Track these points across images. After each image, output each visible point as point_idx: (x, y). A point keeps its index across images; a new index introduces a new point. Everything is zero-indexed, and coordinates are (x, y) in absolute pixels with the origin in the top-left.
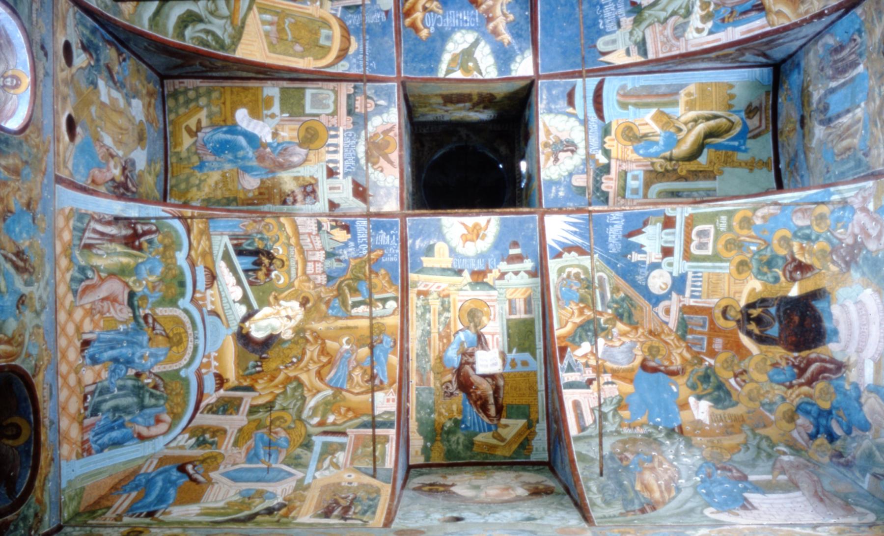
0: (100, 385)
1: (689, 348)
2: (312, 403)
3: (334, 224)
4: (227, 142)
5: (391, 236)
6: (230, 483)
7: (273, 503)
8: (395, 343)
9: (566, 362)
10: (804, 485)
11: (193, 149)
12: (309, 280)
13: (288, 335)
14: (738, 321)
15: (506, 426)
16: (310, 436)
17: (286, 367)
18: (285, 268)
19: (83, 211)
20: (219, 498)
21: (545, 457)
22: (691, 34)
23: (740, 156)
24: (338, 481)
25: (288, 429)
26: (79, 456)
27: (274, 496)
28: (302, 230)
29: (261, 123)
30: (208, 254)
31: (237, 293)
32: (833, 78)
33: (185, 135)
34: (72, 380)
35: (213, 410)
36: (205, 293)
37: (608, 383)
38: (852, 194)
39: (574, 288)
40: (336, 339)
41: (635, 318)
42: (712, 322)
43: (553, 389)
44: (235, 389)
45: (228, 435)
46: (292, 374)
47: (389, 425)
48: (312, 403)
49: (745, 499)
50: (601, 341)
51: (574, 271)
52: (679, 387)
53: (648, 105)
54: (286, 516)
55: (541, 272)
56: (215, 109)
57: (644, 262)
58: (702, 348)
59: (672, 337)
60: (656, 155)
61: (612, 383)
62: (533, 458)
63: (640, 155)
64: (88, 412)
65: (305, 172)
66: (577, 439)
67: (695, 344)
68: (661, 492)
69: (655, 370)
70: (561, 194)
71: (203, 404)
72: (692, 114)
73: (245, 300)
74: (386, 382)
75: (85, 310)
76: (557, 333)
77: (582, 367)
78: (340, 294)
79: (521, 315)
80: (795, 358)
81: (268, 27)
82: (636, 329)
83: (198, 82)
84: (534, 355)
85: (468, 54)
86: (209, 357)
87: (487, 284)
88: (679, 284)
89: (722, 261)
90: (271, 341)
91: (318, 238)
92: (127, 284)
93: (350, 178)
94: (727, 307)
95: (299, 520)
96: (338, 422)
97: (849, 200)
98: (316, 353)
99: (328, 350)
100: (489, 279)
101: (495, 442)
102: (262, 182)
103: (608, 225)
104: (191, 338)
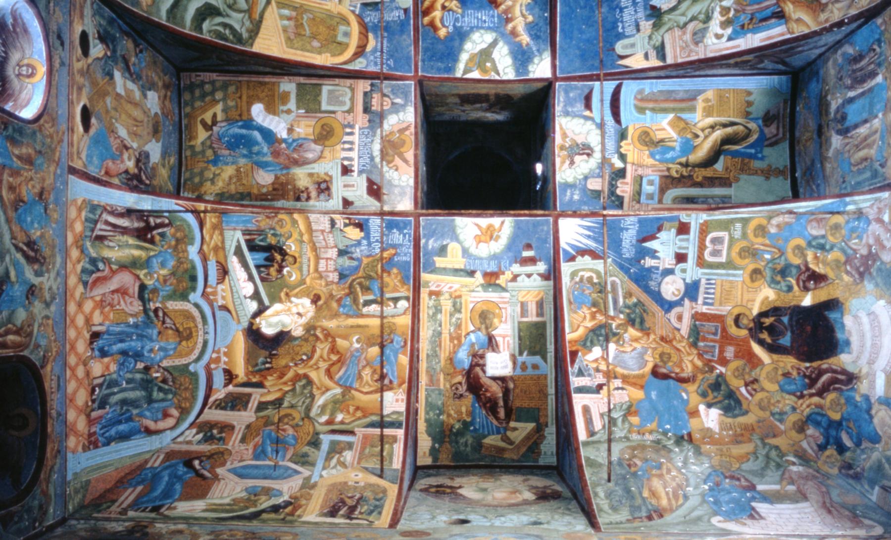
0: (108, 377)
1: (700, 356)
2: (320, 401)
3: (347, 221)
4: (243, 136)
5: (404, 235)
6: (237, 479)
7: (280, 501)
8: (405, 343)
9: (576, 366)
11: (208, 143)
13: (298, 332)
14: (750, 330)
15: (515, 429)
16: (318, 434)
17: (296, 365)
18: (297, 264)
19: (96, 203)
20: (225, 495)
22: (710, 40)
23: (757, 164)
25: (295, 427)
26: (86, 449)
27: (280, 493)
28: (314, 227)
29: (277, 118)
30: (220, 249)
31: (248, 289)
32: (851, 88)
33: (200, 128)
34: (80, 372)
35: (221, 405)
36: (216, 288)
37: (618, 389)
38: (868, 204)
39: (587, 292)
40: (346, 337)
41: (647, 325)
42: (724, 330)
44: (244, 385)
46: (301, 372)
49: (753, 509)
50: (612, 347)
51: (587, 274)
52: (690, 394)
54: (292, 514)
55: (553, 275)
57: (657, 268)
58: (713, 356)
59: (683, 344)
60: (672, 161)
61: (622, 389)
62: (541, 462)
64: (96, 405)
65: (320, 168)
66: (586, 444)
67: (707, 352)
68: (669, 499)
69: (666, 377)
70: (576, 197)
71: (212, 399)
72: (710, 121)
73: (256, 296)
74: (395, 382)
75: (96, 302)
76: (569, 336)
77: (592, 372)
78: (351, 292)
79: (532, 318)
80: (807, 368)
81: (286, 22)
82: (648, 335)
83: (214, 76)
84: (544, 358)
85: (486, 54)
86: (218, 352)
87: (499, 285)
88: (691, 290)
89: (735, 268)
90: (282, 337)
91: (331, 235)
93: (364, 176)
96: (347, 421)
97: (864, 211)
100: (502, 281)
101: (503, 444)
102: (277, 178)
103: (622, 229)
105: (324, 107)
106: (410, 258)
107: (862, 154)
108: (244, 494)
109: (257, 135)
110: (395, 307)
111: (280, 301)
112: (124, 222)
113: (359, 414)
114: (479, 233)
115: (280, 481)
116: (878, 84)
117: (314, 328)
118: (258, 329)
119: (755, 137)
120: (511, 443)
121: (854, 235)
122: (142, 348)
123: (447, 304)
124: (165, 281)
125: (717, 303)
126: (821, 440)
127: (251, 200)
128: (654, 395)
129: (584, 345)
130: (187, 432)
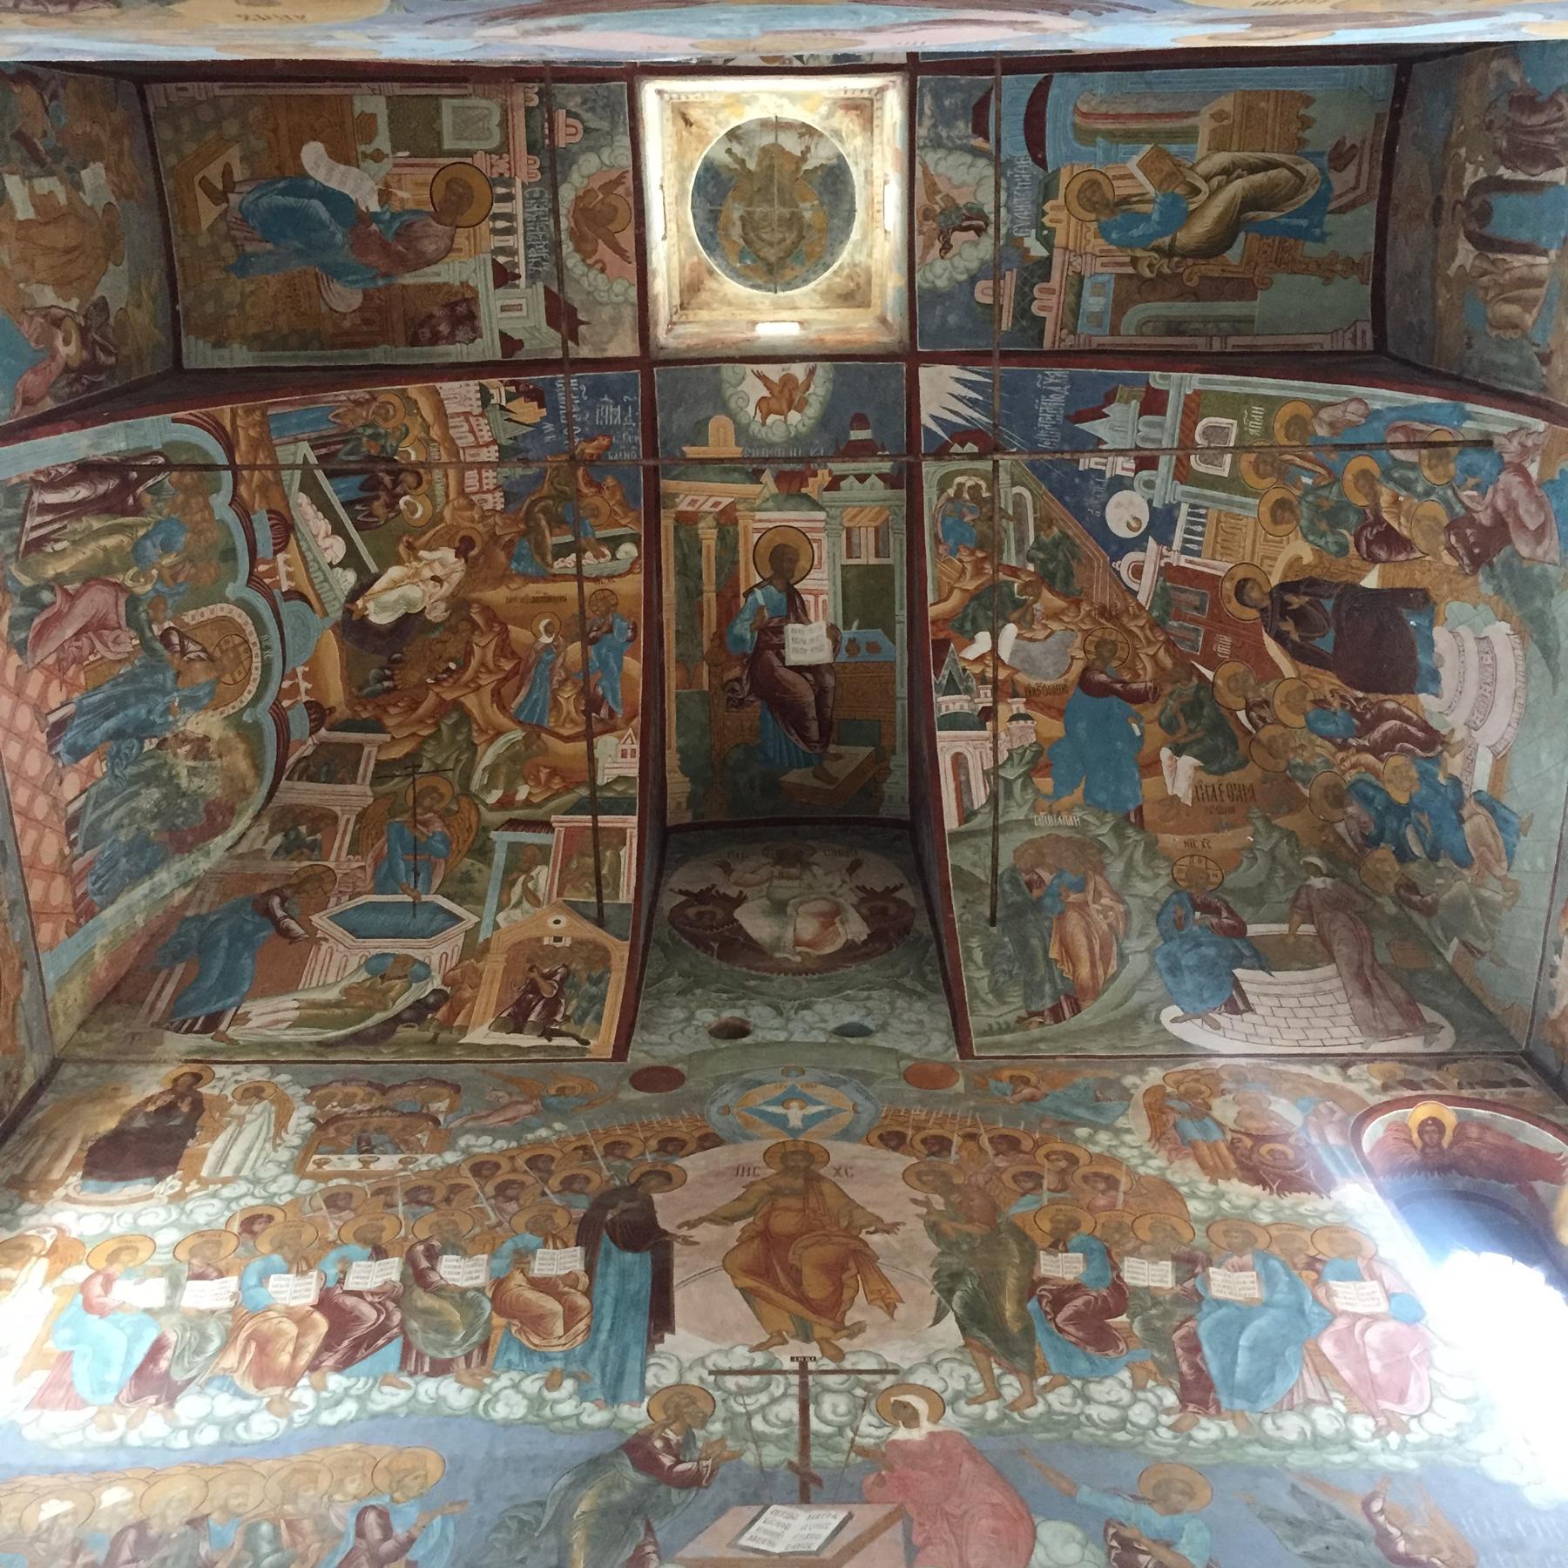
0: (93, 791)
1: (1170, 645)
2: (487, 758)
3: (512, 389)
4: (291, 210)
5: (624, 409)
6: (349, 939)
8: (635, 630)
9: (945, 672)
10: (1341, 950)
11: (222, 227)
12: (472, 505)
13: (437, 614)
14: (1263, 611)
17: (438, 682)
18: (424, 486)
19: (15, 481)
20: (331, 979)
21: (905, 813)
23: (1311, 249)
24: (536, 933)
25: (445, 815)
27: (425, 971)
28: (451, 408)
29: (354, 170)
30: (272, 487)
32: (1507, 159)
33: (203, 201)
35: (310, 770)
36: (274, 560)
37: (1016, 717)
38: (1506, 429)
39: (968, 518)
40: (526, 622)
42: (1216, 602)
43: (922, 726)
45: (342, 823)
46: (449, 696)
47: (619, 806)
48: (487, 758)
49: (1236, 984)
50: (1010, 631)
51: (969, 482)
52: (1145, 725)
53: (1132, 137)
54: (447, 1025)
55: (907, 480)
56: (260, 145)
57: (1101, 473)
58: (1194, 648)
59: (1141, 622)
60: (1143, 243)
61: (1026, 717)
62: (884, 813)
63: (1111, 242)
65: (448, 273)
66: (957, 837)
68: (1093, 965)
69: (1104, 690)
70: (952, 319)
71: (291, 761)
72: (1222, 158)
73: (352, 559)
74: (620, 713)
75: (48, 668)
76: (933, 612)
77: (973, 684)
78: (531, 531)
79: (868, 558)
80: (1358, 700)
82: (1077, 604)
84: (890, 634)
86: (294, 675)
87: (806, 496)
88: (1161, 523)
89: (1245, 494)
90: (410, 624)
91: (483, 421)
92: (120, 587)
93: (540, 287)
94: (1246, 580)
95: (469, 1038)
96: (536, 800)
97: (1496, 440)
98: (490, 655)
99: (515, 647)
100: (812, 488)
101: (817, 783)
102: (367, 296)
104: (256, 650)
105: (448, 145)
107: (1512, 310)
108: (364, 975)
109: (317, 206)
110: (614, 558)
111: (399, 562)
112: (81, 492)
113: (557, 784)
114: (766, 393)
115: (423, 942)
116: (1555, 184)
118: (364, 618)
119: (1311, 193)
121: (1471, 482)
122: (150, 712)
123: (708, 534)
124: (174, 577)
125: (1207, 551)
126: (1372, 830)
127: (322, 348)
128: (1081, 727)
129: (961, 630)
130: (253, 833)
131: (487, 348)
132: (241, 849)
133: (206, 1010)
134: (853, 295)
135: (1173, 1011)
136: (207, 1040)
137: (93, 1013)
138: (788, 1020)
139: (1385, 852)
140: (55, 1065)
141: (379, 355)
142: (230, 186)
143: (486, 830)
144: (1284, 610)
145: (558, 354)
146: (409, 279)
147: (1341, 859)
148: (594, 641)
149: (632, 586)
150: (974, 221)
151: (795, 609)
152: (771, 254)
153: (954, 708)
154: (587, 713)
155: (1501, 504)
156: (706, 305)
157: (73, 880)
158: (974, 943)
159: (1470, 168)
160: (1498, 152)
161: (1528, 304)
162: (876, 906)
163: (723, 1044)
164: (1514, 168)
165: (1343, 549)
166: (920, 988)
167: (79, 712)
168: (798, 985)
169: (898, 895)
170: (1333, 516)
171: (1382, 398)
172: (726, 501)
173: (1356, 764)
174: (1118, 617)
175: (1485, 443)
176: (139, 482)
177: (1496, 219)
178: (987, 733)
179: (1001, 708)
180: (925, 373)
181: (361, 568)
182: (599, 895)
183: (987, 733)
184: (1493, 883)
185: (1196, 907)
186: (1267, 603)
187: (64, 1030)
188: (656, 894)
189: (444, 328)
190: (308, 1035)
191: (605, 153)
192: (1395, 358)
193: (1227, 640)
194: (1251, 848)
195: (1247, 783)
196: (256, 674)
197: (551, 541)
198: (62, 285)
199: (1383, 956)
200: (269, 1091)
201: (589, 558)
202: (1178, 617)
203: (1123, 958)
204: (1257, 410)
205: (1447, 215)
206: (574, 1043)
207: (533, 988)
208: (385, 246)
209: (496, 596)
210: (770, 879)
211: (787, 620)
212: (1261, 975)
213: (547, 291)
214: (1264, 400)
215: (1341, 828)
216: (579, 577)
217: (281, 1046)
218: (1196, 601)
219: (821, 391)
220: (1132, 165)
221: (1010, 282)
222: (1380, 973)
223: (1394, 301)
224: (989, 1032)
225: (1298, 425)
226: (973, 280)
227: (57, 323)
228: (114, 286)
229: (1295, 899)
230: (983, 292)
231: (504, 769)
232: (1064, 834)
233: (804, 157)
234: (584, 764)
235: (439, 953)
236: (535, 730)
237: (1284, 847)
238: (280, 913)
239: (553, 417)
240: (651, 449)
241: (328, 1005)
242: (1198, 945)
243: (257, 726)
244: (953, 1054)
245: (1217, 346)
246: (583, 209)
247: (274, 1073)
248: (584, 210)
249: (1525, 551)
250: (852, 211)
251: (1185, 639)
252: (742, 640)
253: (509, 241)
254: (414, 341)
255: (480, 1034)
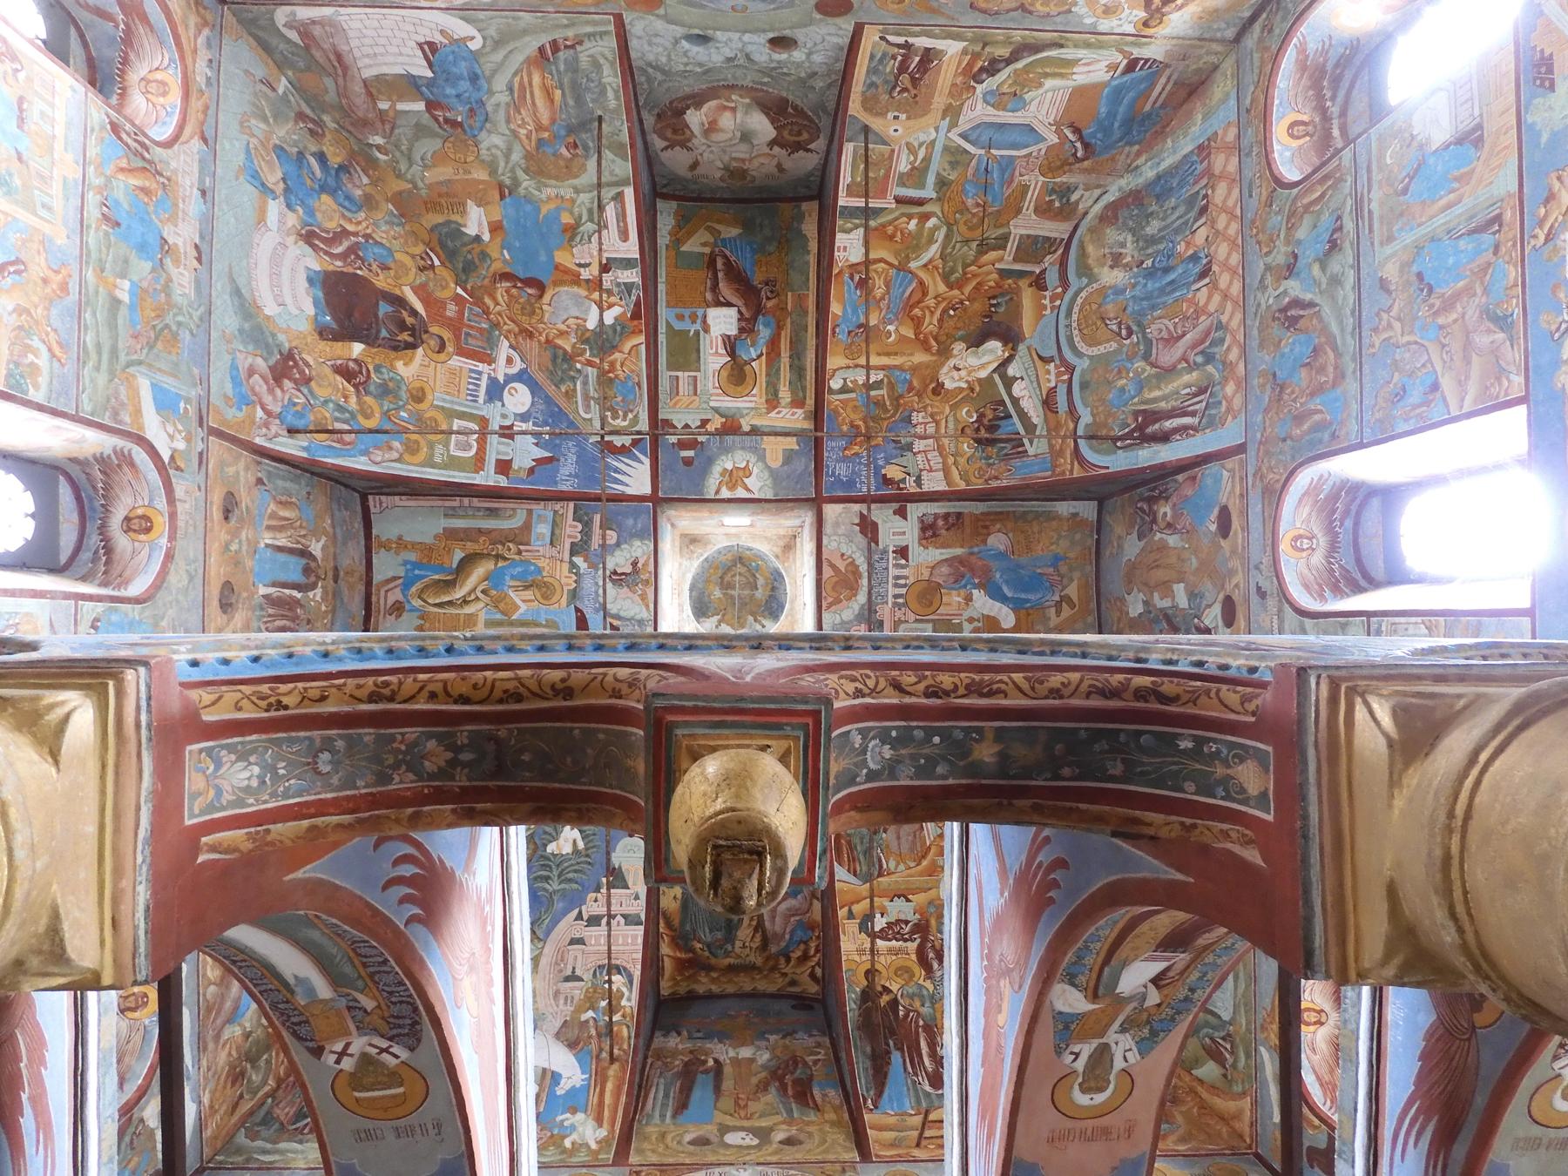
1: (487, 312)
2: (934, 250)
4: (1025, 591)
7: (991, 83)
9: (634, 298)
10: (358, 88)
11: (1065, 581)
12: (932, 416)
13: (958, 347)
14: (426, 332)
15: (704, 244)
20: (1050, 95)
21: (661, 204)
23: (413, 556)
24: (911, 123)
25: (963, 209)
30: (1053, 429)
31: (1018, 389)
32: (297, 602)
33: (1075, 599)
35: (1049, 244)
38: (280, 439)
40: (902, 339)
41: (548, 354)
42: (457, 337)
43: (648, 261)
46: (956, 292)
47: (851, 212)
48: (934, 250)
49: (431, 65)
50: (591, 324)
52: (501, 258)
54: (976, 56)
60: (514, 563)
61: (580, 265)
62: (674, 204)
65: (935, 554)
66: (625, 183)
67: (477, 315)
70: (630, 522)
72: (468, 610)
73: (1009, 382)
76: (642, 338)
77: (615, 290)
78: (896, 399)
82: (548, 341)
86: (1053, 308)
88: (496, 391)
89: (443, 408)
90: (976, 341)
92: (1153, 365)
95: (959, 46)
98: (927, 320)
101: (718, 227)
102: (984, 542)
103: (576, 476)
104: (1074, 325)
106: (829, 445)
109: (1009, 594)
111: (979, 380)
112: (1169, 424)
113: (890, 230)
117: (939, 353)
118: (1005, 344)
119: (414, 589)
120: (709, 229)
121: (299, 408)
123: (785, 394)
124: (1120, 372)
125: (465, 373)
126: (344, 177)
128: (543, 258)
131: (915, 510)
132: (1097, 192)
133: (1133, 75)
134: (691, 541)
135: (475, 45)
136: (1136, 52)
137: (1208, 77)
138: (741, 51)
139: (335, 160)
140: (1238, 39)
141: (979, 508)
142: (1058, 605)
143: (939, 199)
144: (413, 331)
145: (873, 506)
146: (958, 551)
147: (362, 158)
148: (860, 326)
149: (833, 362)
150: (618, 578)
151: (731, 345)
152: (740, 568)
153: (627, 273)
154: (868, 278)
155: (278, 392)
156: (780, 537)
157: (1209, 172)
158: (613, 104)
159: (318, 598)
160: (302, 606)
161: (273, 516)
162: (678, 135)
163: (787, 33)
164: (291, 597)
165: (378, 369)
166: (650, 70)
167: (1189, 285)
168: (734, 77)
169: (665, 144)
170: (385, 391)
171: (360, 463)
172: (773, 414)
173: (359, 223)
174: (521, 331)
175: (292, 431)
176: (1133, 431)
177: (299, 569)
178: (605, 255)
179: (596, 273)
180: (646, 490)
181: (1004, 377)
182: (867, 149)
183: (605, 255)
184: (257, 132)
185: (460, 125)
186: (425, 337)
187: (1228, 66)
188: (828, 152)
189: (940, 523)
190: (1068, 53)
191: (838, 620)
192: (354, 490)
193: (449, 313)
194: (426, 167)
195: (430, 216)
196: (1076, 309)
197: (883, 392)
198: (1163, 547)
199: (329, 82)
200: (1099, 11)
201: (861, 380)
202: (481, 330)
203: (511, 89)
204: (438, 460)
205: (330, 574)
206: (890, 38)
207: (915, 82)
208: (972, 570)
209: (920, 358)
210: (751, 160)
211: (736, 338)
212: (415, 72)
213: (877, 543)
214: (434, 466)
215: (365, 180)
216: (868, 367)
217: (1088, 45)
218: (470, 341)
219: (711, 481)
220: (523, 607)
221: (596, 541)
222: (331, 70)
223: (358, 525)
224: (602, 34)
225: (412, 449)
226: (618, 545)
227: (1169, 525)
228: (1132, 547)
229: (393, 129)
230: (612, 536)
231: (924, 241)
232: (553, 182)
233: (720, 622)
234: (872, 242)
235: (977, 111)
236: (902, 268)
237: (403, 167)
238: (1078, 145)
239: (877, 469)
240: (818, 444)
241: (1054, 75)
242: (458, 96)
243: (1079, 275)
244: (628, 17)
245: (466, 501)
246: (853, 590)
247: (1094, 25)
248: (852, 589)
249: (259, 361)
250: (691, 590)
251: (477, 315)
252: (766, 325)
253: (898, 572)
254: (959, 515)
255: (952, 48)
